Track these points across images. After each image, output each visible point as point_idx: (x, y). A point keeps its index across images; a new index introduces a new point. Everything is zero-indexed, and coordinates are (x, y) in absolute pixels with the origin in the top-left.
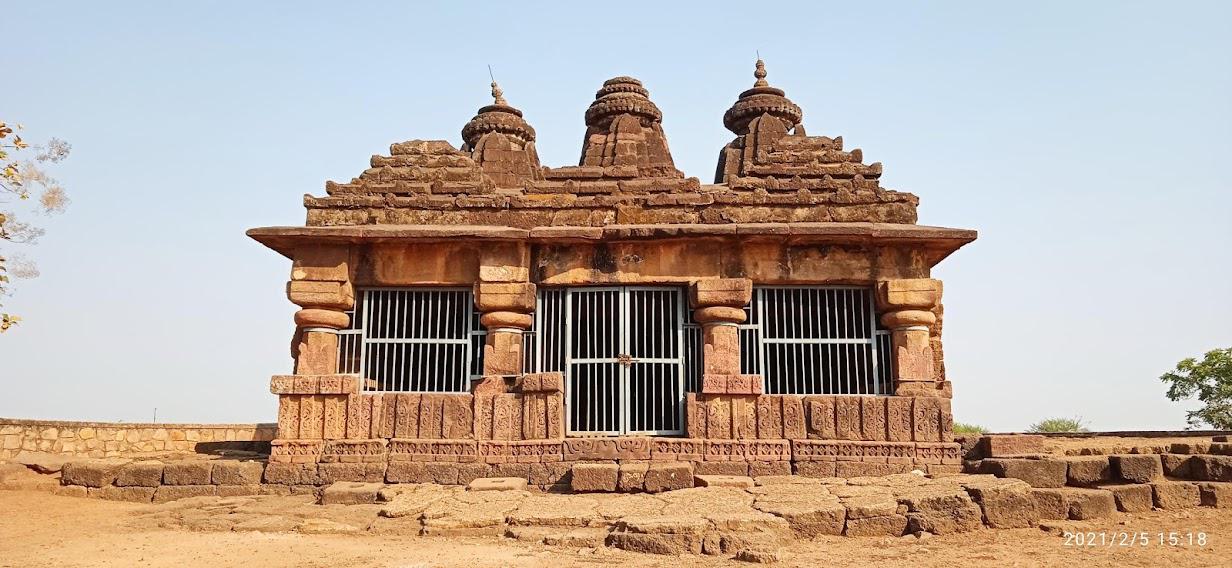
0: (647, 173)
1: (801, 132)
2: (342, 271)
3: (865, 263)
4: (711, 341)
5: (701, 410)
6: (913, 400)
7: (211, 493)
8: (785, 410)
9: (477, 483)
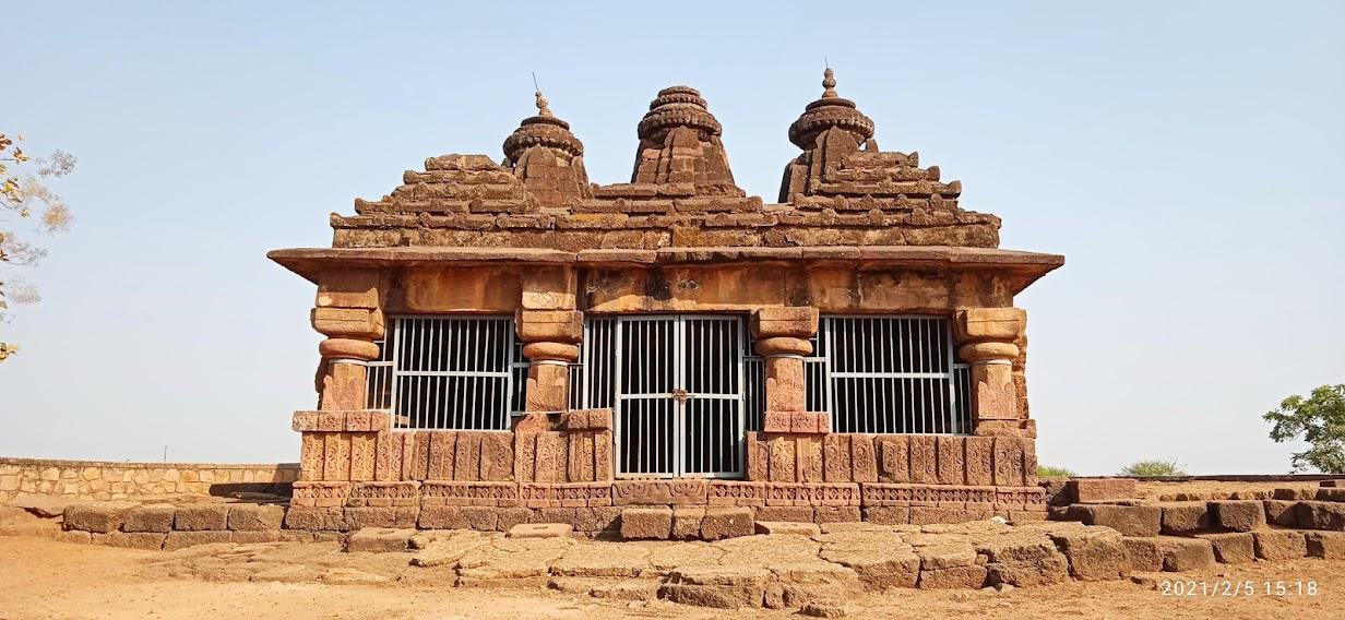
0: (705, 191)
1: (873, 147)
2: (372, 297)
3: (943, 290)
4: (773, 374)
5: (762, 450)
6: (994, 440)
7: (226, 539)
8: (854, 451)
9: (517, 530)
